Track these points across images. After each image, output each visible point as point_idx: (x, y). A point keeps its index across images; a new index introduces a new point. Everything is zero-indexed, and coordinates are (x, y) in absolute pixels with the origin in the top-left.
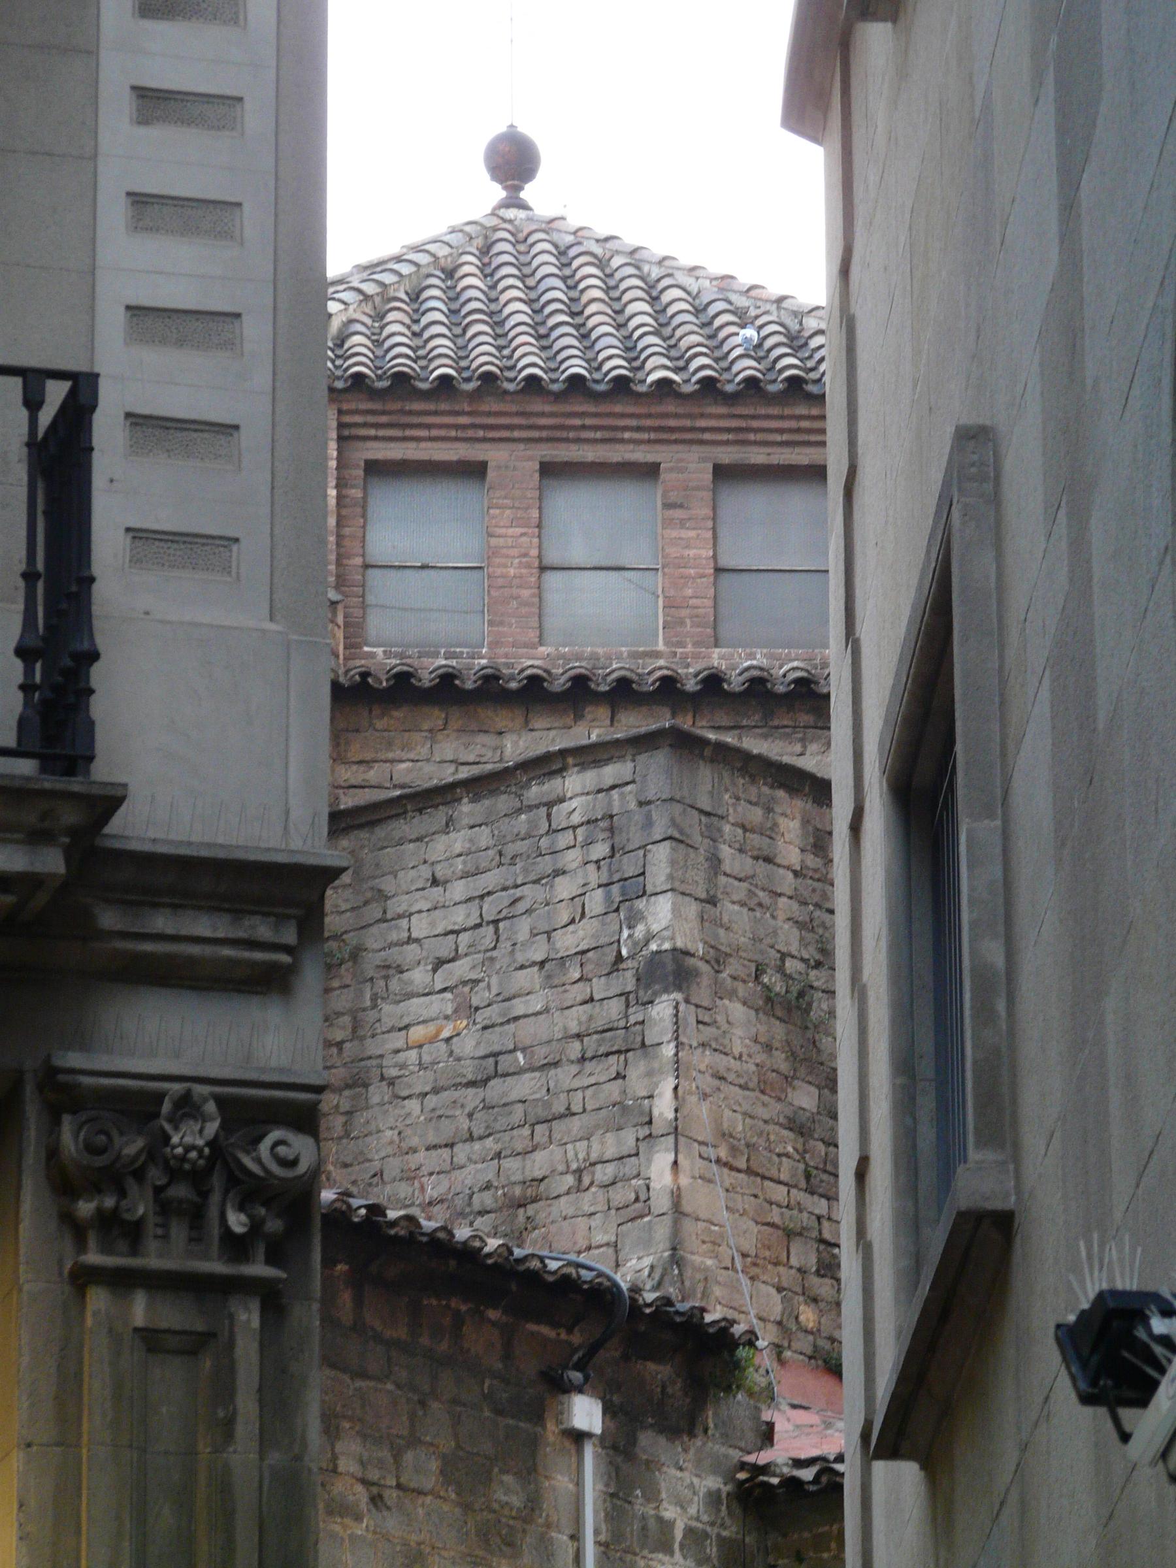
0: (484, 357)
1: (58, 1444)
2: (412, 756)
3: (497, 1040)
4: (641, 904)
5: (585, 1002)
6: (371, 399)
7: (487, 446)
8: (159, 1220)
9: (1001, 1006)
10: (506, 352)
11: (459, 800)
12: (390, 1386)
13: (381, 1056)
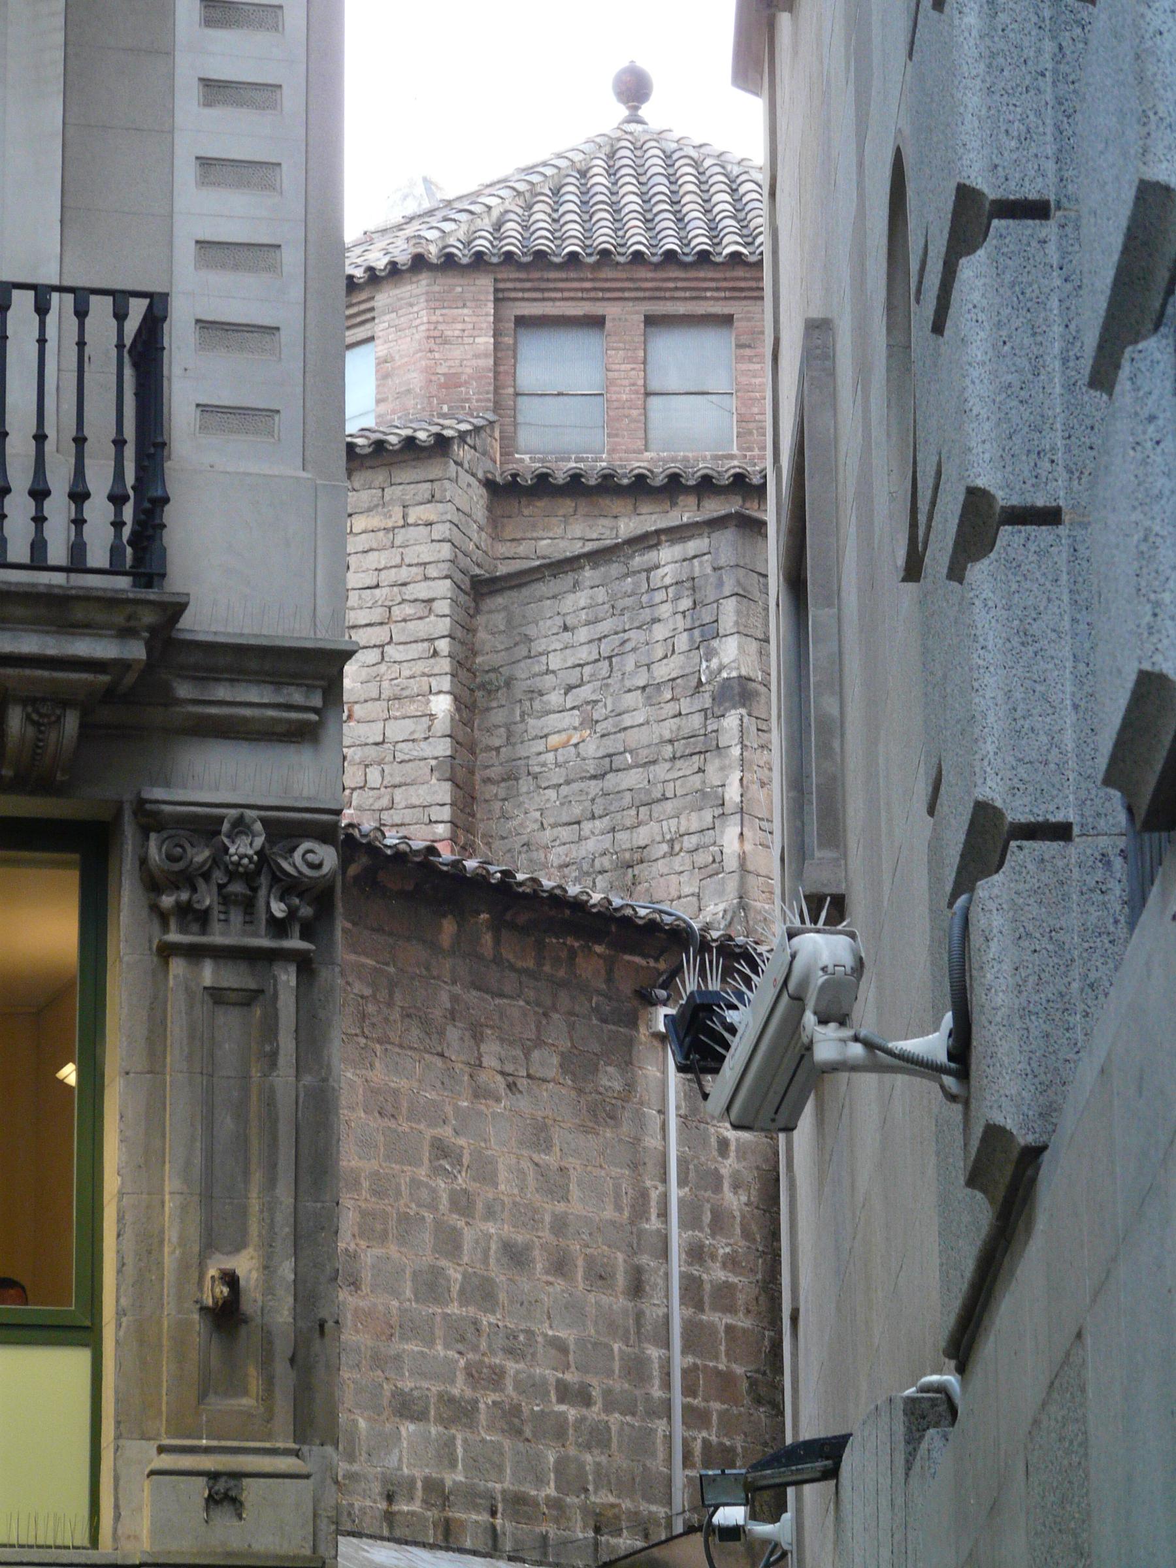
0: (603, 238)
1: (148, 1073)
2: (551, 535)
3: (611, 745)
4: (715, 643)
5: (675, 716)
6: (518, 271)
7: (605, 303)
8: (222, 908)
9: (836, 745)
10: (620, 233)
11: (582, 568)
12: (522, 1003)
13: (528, 757)
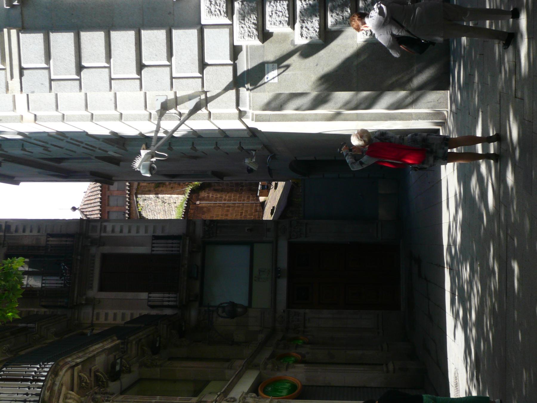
3: (162, 211)
